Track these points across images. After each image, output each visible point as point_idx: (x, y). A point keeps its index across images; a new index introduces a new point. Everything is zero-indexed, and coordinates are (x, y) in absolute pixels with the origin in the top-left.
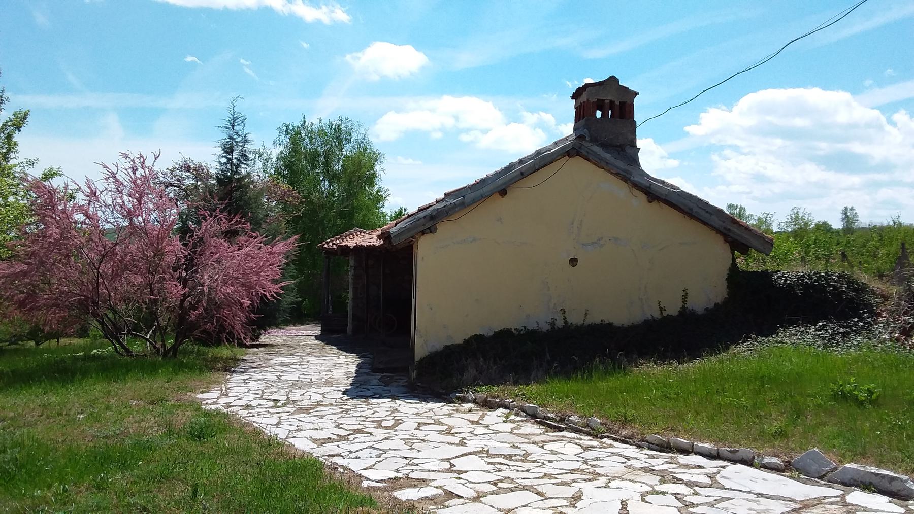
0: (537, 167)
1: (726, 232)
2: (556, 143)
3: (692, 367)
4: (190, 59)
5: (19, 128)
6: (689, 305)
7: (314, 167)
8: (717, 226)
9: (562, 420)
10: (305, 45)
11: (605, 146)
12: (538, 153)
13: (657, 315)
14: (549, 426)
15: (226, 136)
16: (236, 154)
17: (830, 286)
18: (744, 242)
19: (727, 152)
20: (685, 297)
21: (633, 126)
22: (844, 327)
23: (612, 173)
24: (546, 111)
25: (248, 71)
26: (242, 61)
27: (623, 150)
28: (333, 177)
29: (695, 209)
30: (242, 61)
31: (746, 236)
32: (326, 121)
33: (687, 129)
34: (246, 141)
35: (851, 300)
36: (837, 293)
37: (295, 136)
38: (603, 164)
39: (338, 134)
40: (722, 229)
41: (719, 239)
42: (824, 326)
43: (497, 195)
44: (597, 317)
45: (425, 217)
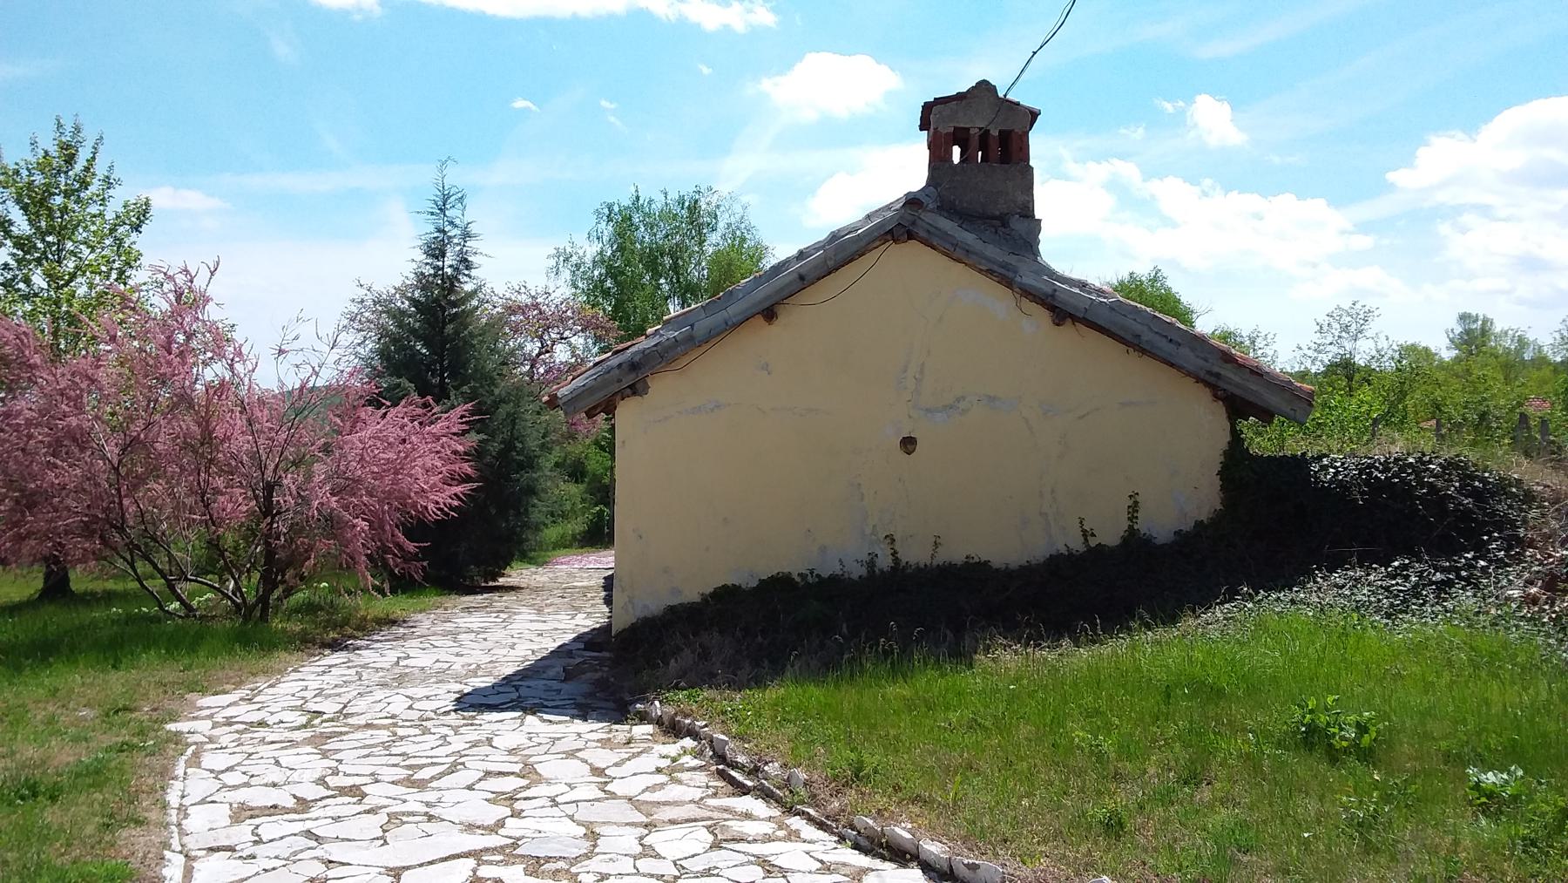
0: (831, 263)
1: (1212, 379)
2: (868, 217)
3: (1114, 650)
4: (520, 104)
5: (136, 228)
6: (1142, 526)
7: (656, 275)
8: (1191, 368)
9: (754, 772)
10: (706, 71)
11: (965, 217)
12: (834, 236)
13: (1077, 545)
14: (732, 781)
15: (432, 228)
16: (450, 259)
17: (1422, 485)
18: (1251, 399)
19: (1467, 219)
20: (1134, 508)
21: (1028, 172)
22: (1443, 570)
23: (980, 271)
24: (1122, 157)
25: (612, 119)
26: (604, 103)
27: (1005, 224)
28: (687, 291)
29: (1147, 336)
30: (604, 103)
31: (1253, 386)
32: (673, 195)
33: (1391, 176)
34: (466, 235)
35: (1466, 514)
36: (1437, 499)
37: (623, 223)
38: (959, 253)
39: (694, 217)
40: (1202, 374)
41: (1205, 394)
42: (1404, 567)
43: (760, 320)
44: (955, 552)
45: (620, 365)
